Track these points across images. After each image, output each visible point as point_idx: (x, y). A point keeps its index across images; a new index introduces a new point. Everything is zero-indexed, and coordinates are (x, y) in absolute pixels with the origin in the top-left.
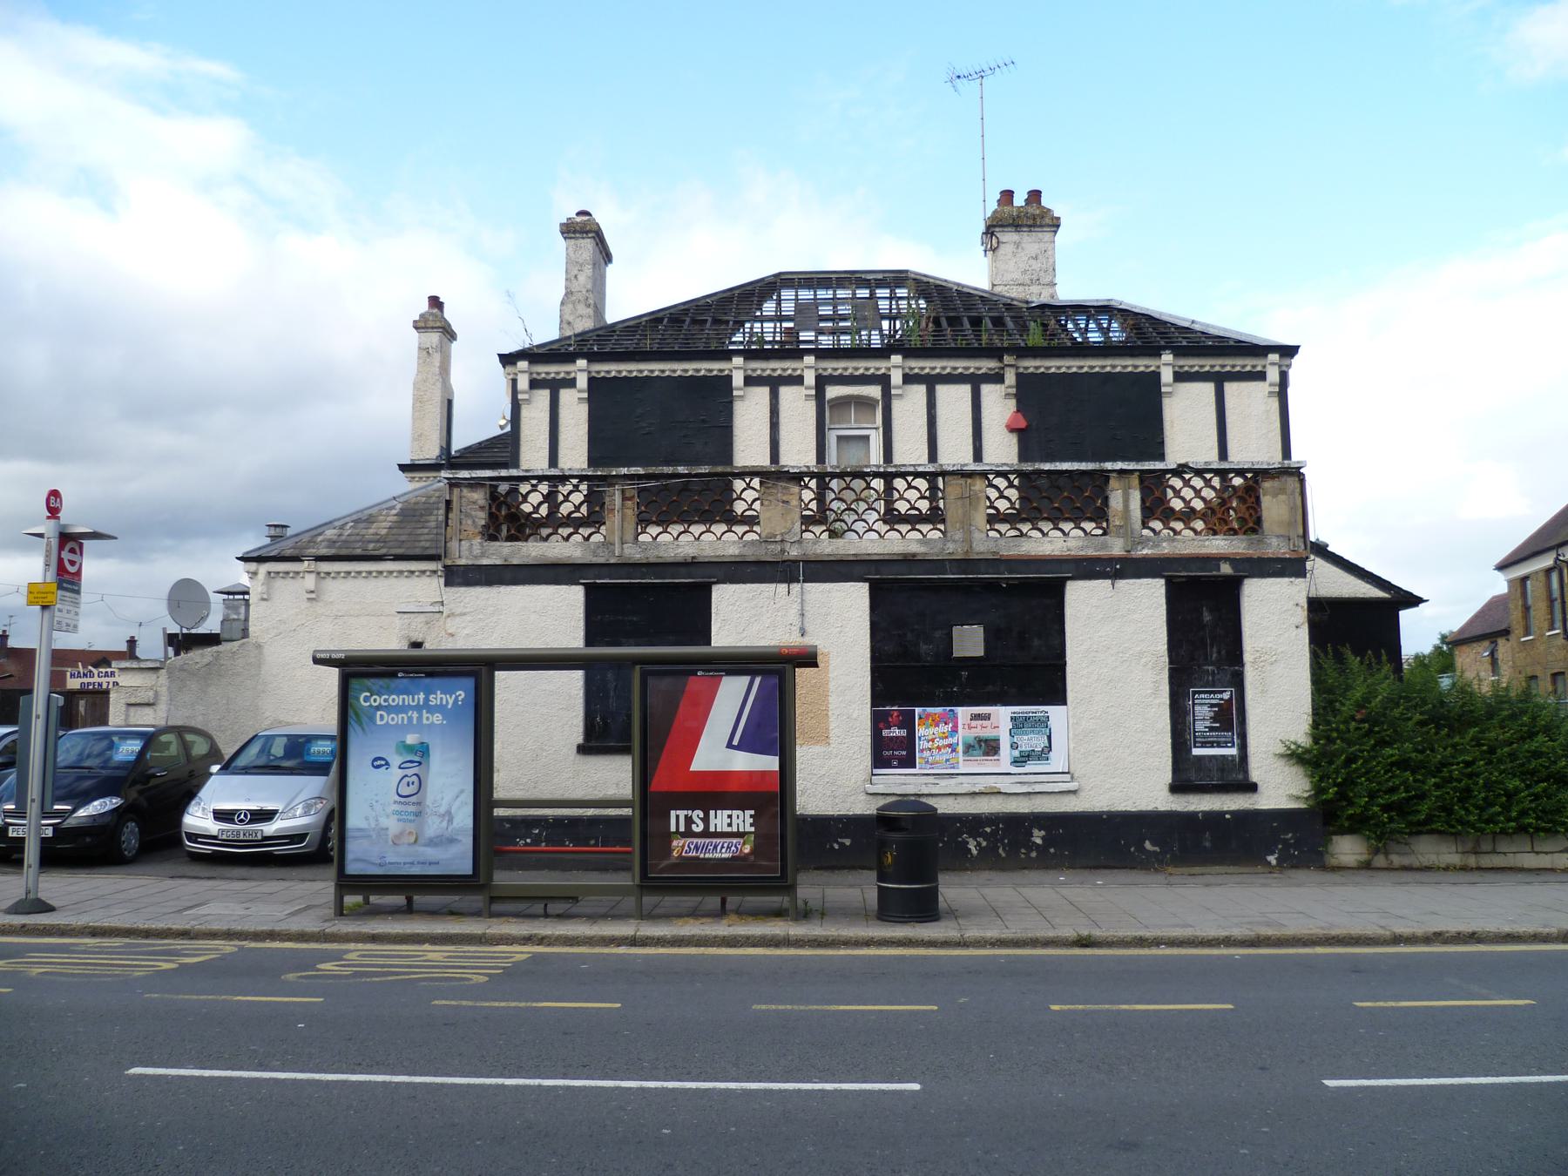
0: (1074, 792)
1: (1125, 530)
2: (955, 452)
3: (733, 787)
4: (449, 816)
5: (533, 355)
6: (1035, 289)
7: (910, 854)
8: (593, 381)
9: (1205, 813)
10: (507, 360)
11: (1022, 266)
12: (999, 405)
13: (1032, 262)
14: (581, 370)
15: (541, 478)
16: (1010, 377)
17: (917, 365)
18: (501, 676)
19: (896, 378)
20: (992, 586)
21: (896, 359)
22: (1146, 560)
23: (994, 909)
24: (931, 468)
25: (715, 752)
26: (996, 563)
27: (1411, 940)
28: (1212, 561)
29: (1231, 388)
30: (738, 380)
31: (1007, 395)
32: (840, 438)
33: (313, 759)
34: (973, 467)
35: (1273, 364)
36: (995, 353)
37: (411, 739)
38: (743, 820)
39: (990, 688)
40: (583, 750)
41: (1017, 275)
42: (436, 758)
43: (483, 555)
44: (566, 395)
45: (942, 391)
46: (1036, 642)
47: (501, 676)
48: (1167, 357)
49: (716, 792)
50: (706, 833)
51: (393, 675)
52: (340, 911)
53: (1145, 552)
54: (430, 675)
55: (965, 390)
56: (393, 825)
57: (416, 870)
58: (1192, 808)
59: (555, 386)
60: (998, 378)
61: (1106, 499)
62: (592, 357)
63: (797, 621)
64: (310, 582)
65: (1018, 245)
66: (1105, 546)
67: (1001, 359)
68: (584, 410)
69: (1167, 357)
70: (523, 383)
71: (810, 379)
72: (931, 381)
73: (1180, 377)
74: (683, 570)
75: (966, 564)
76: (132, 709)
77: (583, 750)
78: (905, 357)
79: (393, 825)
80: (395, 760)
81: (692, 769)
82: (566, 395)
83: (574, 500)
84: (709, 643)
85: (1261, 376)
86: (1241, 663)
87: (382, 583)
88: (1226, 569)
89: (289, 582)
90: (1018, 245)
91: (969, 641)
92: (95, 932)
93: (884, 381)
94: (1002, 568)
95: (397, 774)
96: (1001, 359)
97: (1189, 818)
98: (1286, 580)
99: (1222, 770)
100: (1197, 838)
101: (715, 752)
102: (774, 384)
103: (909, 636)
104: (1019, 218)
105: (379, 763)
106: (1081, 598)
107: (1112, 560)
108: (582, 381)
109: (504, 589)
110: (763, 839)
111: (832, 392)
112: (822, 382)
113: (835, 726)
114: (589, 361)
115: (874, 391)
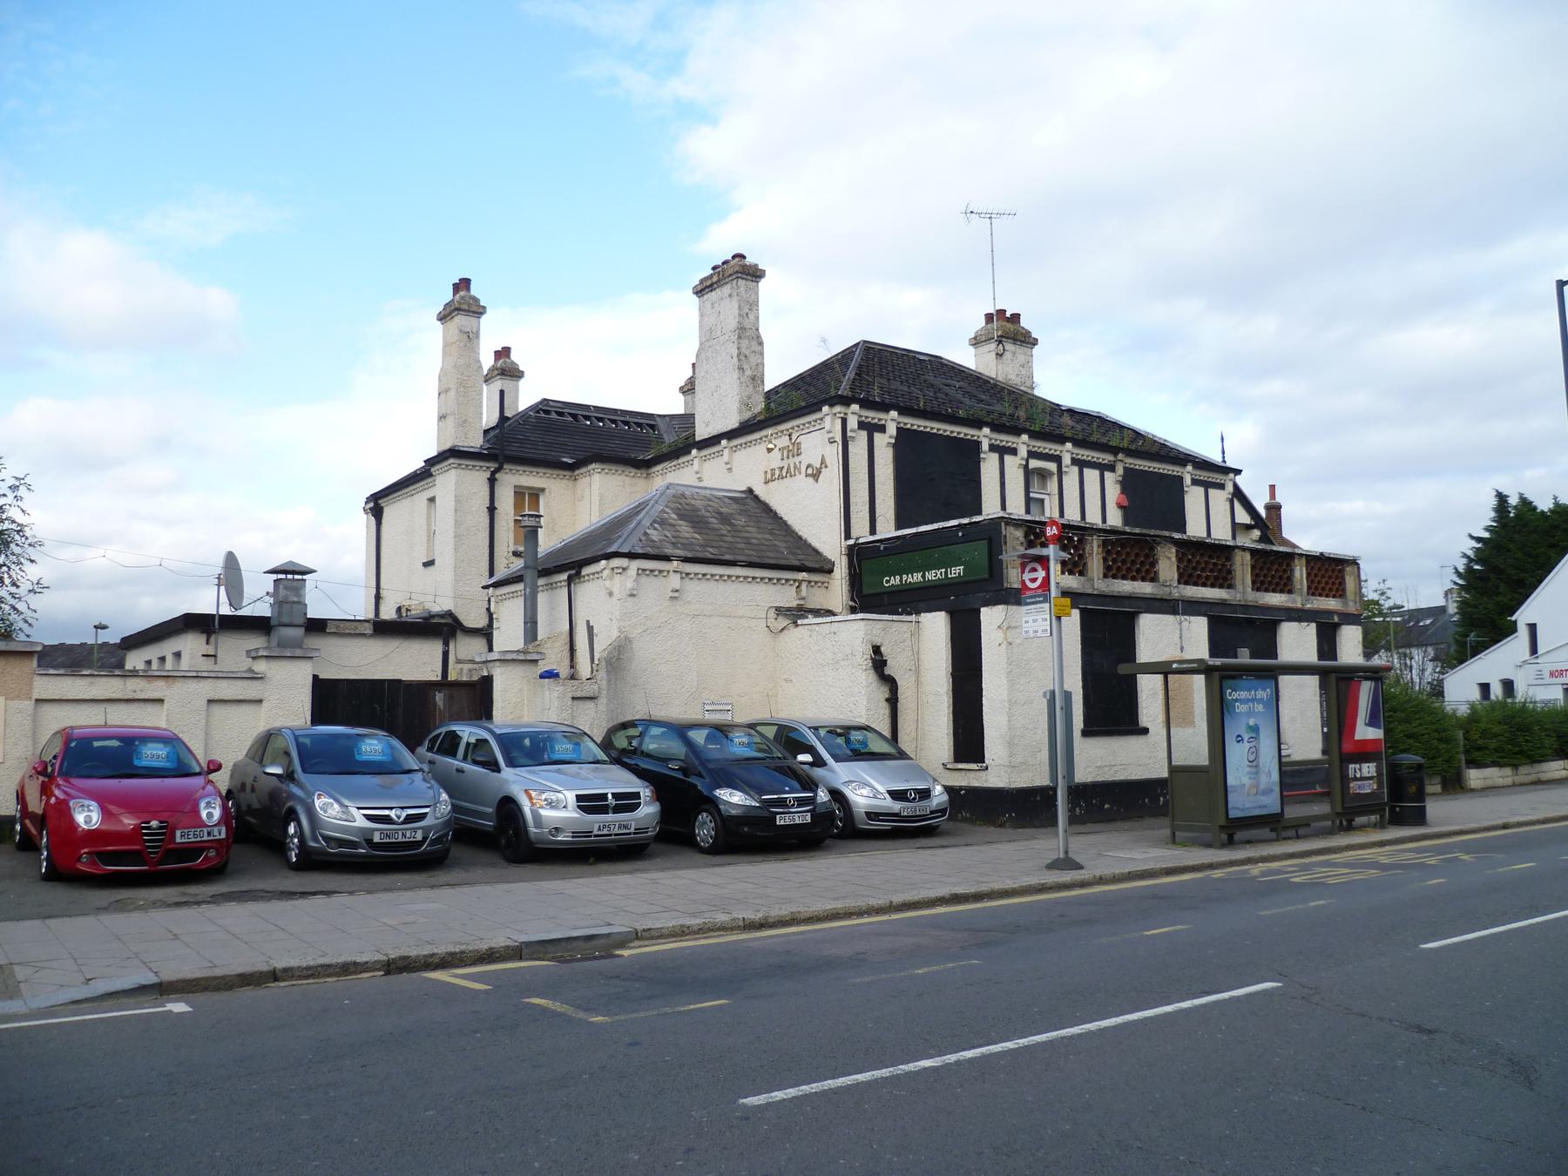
16: (1120, 470)
17: (1203, 475)
19: (1067, 460)
20: (1250, 622)
21: (855, 407)
29: (1211, 491)
30: (1188, 480)
33: (365, 758)
34: (1101, 526)
36: (1115, 451)
37: (1252, 722)
38: (1369, 769)
42: (1262, 733)
56: (1246, 780)
57: (1257, 812)
59: (871, 429)
60: (1112, 468)
61: (1292, 571)
62: (903, 411)
63: (1177, 640)
64: (675, 581)
65: (1014, 354)
66: (1294, 601)
67: (1116, 455)
70: (853, 423)
76: (218, 710)
78: (831, 406)
79: (1246, 780)
80: (1246, 737)
84: (1275, 657)
87: (731, 588)
88: (1336, 619)
89: (652, 579)
90: (1014, 354)
93: (1058, 459)
95: (1247, 745)
96: (1116, 455)
102: (1002, 451)
104: (1007, 330)
105: (1239, 739)
108: (892, 429)
112: (1032, 454)
115: (1052, 466)
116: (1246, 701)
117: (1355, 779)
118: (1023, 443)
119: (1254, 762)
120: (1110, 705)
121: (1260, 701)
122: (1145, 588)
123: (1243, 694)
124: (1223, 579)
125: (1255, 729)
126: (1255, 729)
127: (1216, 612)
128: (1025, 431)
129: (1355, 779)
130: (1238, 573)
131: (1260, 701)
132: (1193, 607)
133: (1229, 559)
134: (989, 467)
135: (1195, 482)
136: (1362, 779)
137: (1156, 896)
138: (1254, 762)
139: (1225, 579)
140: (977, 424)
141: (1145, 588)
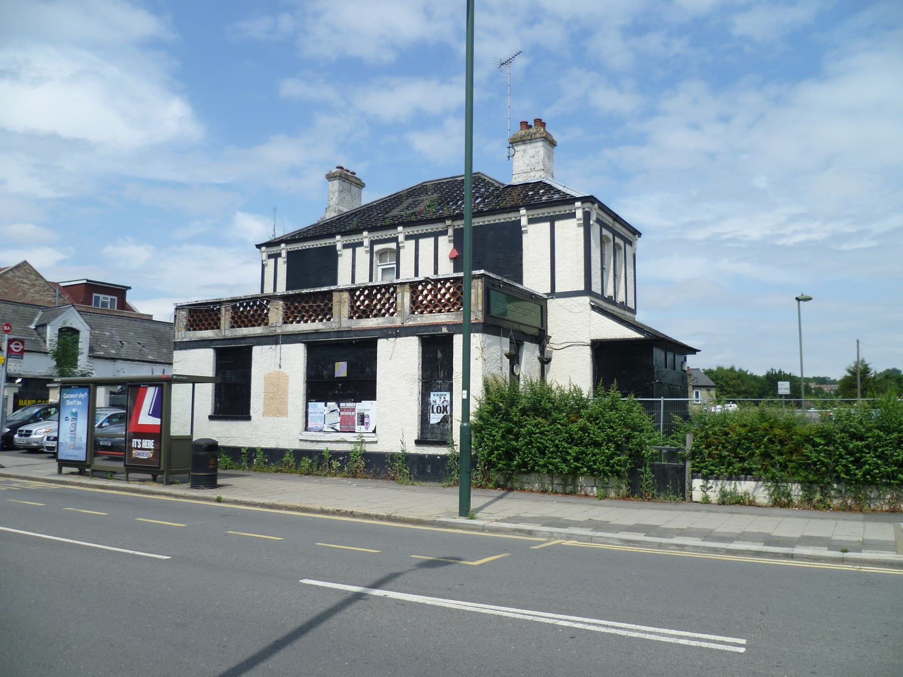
0: (376, 442)
1: (402, 313)
2: (426, 271)
3: (147, 431)
4: (81, 438)
5: (268, 244)
6: (532, 174)
7: (204, 464)
8: (289, 253)
9: (430, 456)
10: (259, 246)
11: (527, 162)
12: (446, 246)
13: (532, 159)
14: (284, 249)
15: (366, 288)
17: (411, 230)
18: (175, 387)
19: (401, 238)
20: (349, 343)
22: (410, 327)
23: (245, 490)
24: (435, 277)
25: (145, 419)
26: (349, 331)
27: (327, 512)
28: (438, 326)
30: (339, 246)
31: (579, 225)
32: (383, 270)
35: (579, 208)
36: (441, 219)
37: (74, 410)
38: (149, 444)
39: (349, 392)
40: (211, 418)
41: (524, 168)
43: (185, 337)
44: (280, 260)
45: (421, 241)
46: (368, 370)
47: (175, 387)
48: (523, 211)
49: (144, 433)
50: (141, 449)
51: (70, 387)
52: (60, 472)
53: (411, 323)
54: (80, 387)
55: (431, 240)
56: (68, 440)
58: (424, 453)
59: (276, 256)
60: (445, 233)
63: (278, 360)
65: (524, 151)
66: (393, 321)
68: (285, 266)
69: (523, 211)
70: (265, 256)
71: (366, 242)
72: (416, 238)
73: (531, 221)
74: (345, 334)
75: (339, 333)
77: (211, 418)
78: (404, 227)
79: (68, 440)
80: (70, 418)
81: (140, 422)
82: (359, 250)
83: (446, 293)
85: (572, 215)
86: (452, 379)
88: (445, 330)
90: (524, 151)
91: (341, 369)
92: (18, 477)
93: (395, 240)
94: (352, 334)
97: (421, 458)
98: (268, 347)
99: (442, 434)
100: (419, 470)
101: (145, 419)
102: (354, 246)
103: (320, 367)
105: (67, 419)
106: (384, 346)
107: (396, 328)
108: (284, 254)
109: (191, 351)
110: (157, 451)
111: (377, 248)
112: (373, 243)
113: (290, 408)
114: (453, 221)
115: (393, 245)
116: (71, 399)
117: (137, 449)
118: (366, 237)
119: (73, 432)
120: (233, 400)
121: (80, 399)
122: (258, 330)
123: (72, 396)
124: (216, 325)
125: (75, 414)
126: (75, 414)
127: (312, 339)
128: (365, 229)
129: (137, 449)
130: (222, 321)
131: (80, 399)
132: (290, 338)
133: (331, 300)
134: (345, 257)
135: (345, 246)
136: (141, 449)
137: (346, 526)
138: (73, 432)
139: (192, 326)
140: (333, 236)
141: (258, 330)
